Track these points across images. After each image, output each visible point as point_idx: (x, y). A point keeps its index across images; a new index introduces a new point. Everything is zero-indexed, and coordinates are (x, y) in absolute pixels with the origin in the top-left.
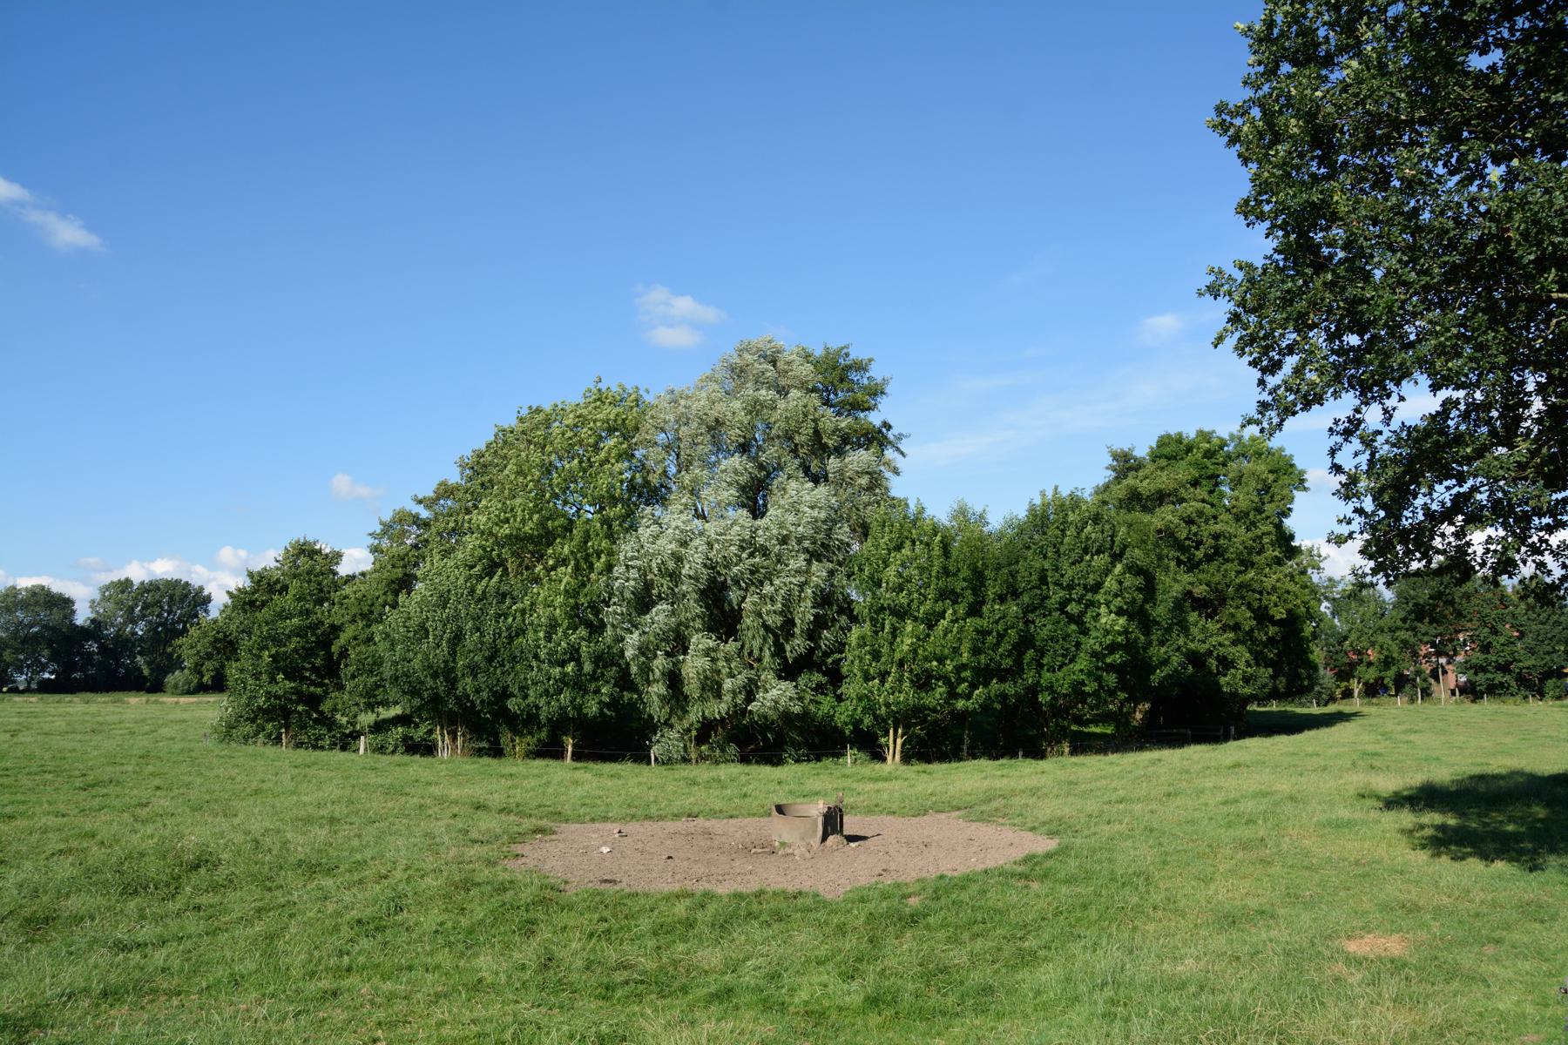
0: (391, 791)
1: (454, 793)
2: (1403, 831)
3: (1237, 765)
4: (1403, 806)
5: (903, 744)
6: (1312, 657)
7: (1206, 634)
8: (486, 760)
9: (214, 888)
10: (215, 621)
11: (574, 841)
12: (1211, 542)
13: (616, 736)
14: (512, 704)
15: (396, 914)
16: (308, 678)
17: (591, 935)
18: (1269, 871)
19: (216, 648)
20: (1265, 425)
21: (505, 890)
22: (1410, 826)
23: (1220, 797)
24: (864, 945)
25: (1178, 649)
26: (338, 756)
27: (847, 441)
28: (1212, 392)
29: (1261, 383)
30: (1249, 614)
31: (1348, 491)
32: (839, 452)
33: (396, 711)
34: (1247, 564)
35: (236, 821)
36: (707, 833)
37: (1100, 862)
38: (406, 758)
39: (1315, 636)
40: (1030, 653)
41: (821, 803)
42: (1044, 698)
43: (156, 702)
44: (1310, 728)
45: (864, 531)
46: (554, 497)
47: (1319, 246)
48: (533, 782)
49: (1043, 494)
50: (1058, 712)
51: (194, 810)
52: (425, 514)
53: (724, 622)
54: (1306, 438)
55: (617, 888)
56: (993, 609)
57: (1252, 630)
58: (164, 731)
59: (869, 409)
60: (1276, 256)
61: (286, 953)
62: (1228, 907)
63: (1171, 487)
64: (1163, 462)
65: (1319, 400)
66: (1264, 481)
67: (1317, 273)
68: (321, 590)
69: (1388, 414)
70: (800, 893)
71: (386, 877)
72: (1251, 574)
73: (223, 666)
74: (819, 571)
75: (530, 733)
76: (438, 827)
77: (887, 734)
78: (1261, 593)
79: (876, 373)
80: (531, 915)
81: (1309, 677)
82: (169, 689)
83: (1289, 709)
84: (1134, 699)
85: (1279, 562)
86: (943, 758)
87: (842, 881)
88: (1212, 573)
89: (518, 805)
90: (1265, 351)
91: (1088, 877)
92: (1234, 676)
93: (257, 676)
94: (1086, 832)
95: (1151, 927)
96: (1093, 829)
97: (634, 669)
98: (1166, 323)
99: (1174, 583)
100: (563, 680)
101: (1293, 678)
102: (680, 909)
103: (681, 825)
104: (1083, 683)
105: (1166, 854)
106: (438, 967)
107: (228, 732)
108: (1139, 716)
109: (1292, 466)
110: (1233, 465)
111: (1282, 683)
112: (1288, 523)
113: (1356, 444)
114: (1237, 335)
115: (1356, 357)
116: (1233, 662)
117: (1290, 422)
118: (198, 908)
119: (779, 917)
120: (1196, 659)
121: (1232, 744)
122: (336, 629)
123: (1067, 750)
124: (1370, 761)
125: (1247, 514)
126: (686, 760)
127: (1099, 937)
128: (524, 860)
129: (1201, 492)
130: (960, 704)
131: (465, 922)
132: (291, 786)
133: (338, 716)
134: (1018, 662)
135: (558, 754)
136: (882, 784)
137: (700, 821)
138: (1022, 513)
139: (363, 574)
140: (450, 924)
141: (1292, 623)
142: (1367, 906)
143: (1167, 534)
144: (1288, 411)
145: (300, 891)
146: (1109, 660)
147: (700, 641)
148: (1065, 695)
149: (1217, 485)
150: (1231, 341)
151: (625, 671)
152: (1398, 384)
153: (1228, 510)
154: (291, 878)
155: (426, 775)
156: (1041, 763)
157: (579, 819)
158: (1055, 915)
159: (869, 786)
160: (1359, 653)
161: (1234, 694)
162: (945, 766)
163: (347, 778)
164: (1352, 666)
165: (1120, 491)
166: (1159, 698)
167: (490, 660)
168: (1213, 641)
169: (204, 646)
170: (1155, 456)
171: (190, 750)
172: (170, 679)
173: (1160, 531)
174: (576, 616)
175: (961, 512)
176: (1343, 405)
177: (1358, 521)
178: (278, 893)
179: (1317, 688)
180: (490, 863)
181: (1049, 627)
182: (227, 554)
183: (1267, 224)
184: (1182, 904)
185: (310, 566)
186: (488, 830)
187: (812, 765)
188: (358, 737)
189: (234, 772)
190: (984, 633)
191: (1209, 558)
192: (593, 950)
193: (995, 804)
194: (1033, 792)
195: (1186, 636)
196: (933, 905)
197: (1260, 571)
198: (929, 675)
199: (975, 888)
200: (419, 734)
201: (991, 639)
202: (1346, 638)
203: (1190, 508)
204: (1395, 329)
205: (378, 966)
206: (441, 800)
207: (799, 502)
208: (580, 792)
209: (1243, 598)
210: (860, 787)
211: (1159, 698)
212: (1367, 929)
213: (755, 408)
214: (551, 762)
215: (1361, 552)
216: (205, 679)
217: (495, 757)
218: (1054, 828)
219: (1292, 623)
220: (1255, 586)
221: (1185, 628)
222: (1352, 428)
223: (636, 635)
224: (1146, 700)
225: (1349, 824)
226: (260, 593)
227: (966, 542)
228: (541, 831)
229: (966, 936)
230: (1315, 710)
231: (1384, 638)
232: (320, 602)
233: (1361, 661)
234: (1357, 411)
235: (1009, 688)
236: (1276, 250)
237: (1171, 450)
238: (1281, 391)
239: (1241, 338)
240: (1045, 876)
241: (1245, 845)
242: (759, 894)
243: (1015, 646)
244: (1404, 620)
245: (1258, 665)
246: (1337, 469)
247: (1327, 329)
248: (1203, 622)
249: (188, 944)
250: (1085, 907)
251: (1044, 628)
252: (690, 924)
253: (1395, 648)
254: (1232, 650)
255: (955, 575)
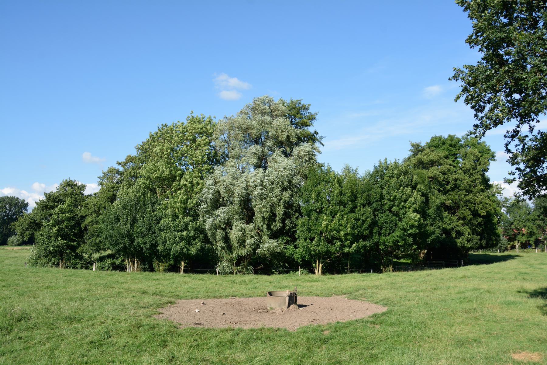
0: (107, 286)
1: (133, 287)
2: (538, 307)
3: (464, 277)
4: (538, 296)
5: (322, 267)
6: (497, 231)
7: (451, 221)
8: (147, 273)
9: (27, 329)
10: (30, 214)
11: (184, 307)
12: (453, 182)
13: (202, 263)
14: (160, 248)
15: (108, 338)
16: (72, 239)
17: (191, 347)
18: (478, 322)
19: (30, 226)
20: (478, 134)
21: (154, 328)
22: (542, 305)
23: (457, 290)
24: (305, 351)
25: (439, 227)
26: (84, 271)
27: (301, 139)
28: (457, 120)
29: (476, 116)
30: (470, 213)
31: (513, 160)
32: (297, 144)
33: (109, 252)
34: (469, 192)
35: (38, 300)
36: (240, 304)
37: (405, 317)
38: (113, 272)
39: (499, 222)
40: (376, 229)
41: (287, 291)
42: (382, 247)
43: (3, 249)
44: (496, 261)
45: (305, 177)
46: (171, 163)
47: (502, 56)
48: (167, 282)
49: (380, 162)
50: (389, 253)
51: (19, 295)
52: (121, 169)
53: (248, 214)
54: (495, 138)
55: (202, 327)
56: (360, 211)
57: (471, 220)
58: (7, 262)
59: (309, 126)
60: (483, 61)
61: (59, 356)
62: (460, 338)
63: (437, 158)
64: (433, 148)
65: (501, 122)
66: (477, 156)
67: (501, 67)
68: (77, 201)
69: (531, 129)
70: (279, 329)
71: (104, 323)
72: (471, 196)
73: (33, 234)
74: (286, 195)
75: (166, 261)
76: (126, 301)
77: (315, 263)
78: (475, 204)
79: (312, 111)
80: (166, 338)
81: (496, 240)
82: (9, 244)
83: (487, 253)
84: (420, 248)
85: (483, 191)
86: (339, 272)
87: (296, 324)
88: (454, 195)
89: (160, 292)
90: (477, 102)
91: (400, 323)
92: (463, 239)
93: (49, 237)
94: (399, 304)
95: (427, 345)
96: (402, 303)
97: (209, 235)
98: (435, 89)
99: (437, 199)
100: (182, 239)
101: (489, 240)
102: (228, 336)
103: (229, 300)
104: (398, 241)
105: (433, 314)
106: (125, 361)
107: (35, 262)
108: (422, 255)
109: (489, 150)
110: (463, 150)
111: (484, 242)
112: (487, 174)
113: (517, 141)
114: (465, 96)
115: (517, 104)
116: (462, 233)
117: (488, 132)
118: (20, 338)
119: (270, 339)
120: (446, 232)
121: (462, 268)
122: (83, 218)
123: (391, 269)
124: (524, 276)
125: (469, 170)
126: (232, 273)
127: (405, 349)
128: (162, 315)
129: (450, 161)
130: (346, 250)
131: (137, 342)
132: (63, 284)
133: (84, 255)
134: (371, 232)
135: (178, 270)
136: (313, 284)
137: (237, 299)
138: (372, 170)
139: (95, 194)
140: (131, 343)
141: (488, 217)
142: (522, 339)
143: (434, 179)
144: (488, 128)
145: (65, 328)
146: (409, 232)
147: (238, 224)
148: (391, 247)
149: (456, 158)
150: (463, 98)
151: (206, 235)
152: (536, 115)
153: (461, 169)
154: (63, 324)
155: (121, 279)
156: (380, 275)
157: (186, 298)
158: (386, 340)
159: (308, 284)
160: (519, 230)
161: (463, 247)
162: (340, 276)
163: (87, 281)
164: (515, 235)
165: (414, 160)
166: (430, 248)
167: (149, 230)
168: (454, 224)
169: (25, 225)
170: (429, 146)
171: (19, 270)
172: (10, 239)
173: (431, 178)
174: (186, 212)
175: (347, 170)
176: (511, 125)
177: (518, 173)
178: (56, 331)
179: (499, 245)
180: (148, 316)
181: (384, 217)
182: (36, 186)
183: (480, 47)
184: (440, 335)
185: (72, 190)
186: (148, 302)
187: (285, 275)
188: (92, 264)
189: (38, 279)
190: (357, 220)
191: (452, 189)
192: (191, 353)
193: (361, 292)
194: (377, 287)
195: (443, 222)
196: (335, 334)
197: (475, 195)
198: (333, 238)
199: (352, 328)
200: (118, 262)
201: (359, 223)
202: (512, 223)
203: (445, 168)
204: (536, 91)
205: (99, 361)
206: (127, 290)
207: (281, 165)
208: (187, 286)
209: (467, 206)
210: (304, 284)
211: (430, 248)
212: (523, 349)
213: (262, 123)
214: (175, 274)
215: (518, 186)
216: (25, 239)
217: (151, 271)
218: (386, 302)
219: (488, 217)
220: (473, 201)
221: (441, 218)
222: (515, 134)
223: (211, 220)
224: (425, 249)
225: (514, 303)
226: (51, 202)
227: (349, 182)
228: (170, 303)
229: (348, 348)
230: (499, 254)
231: (530, 224)
232: (76, 206)
233: (519, 233)
234: (518, 127)
235: (367, 243)
236: (483, 59)
237: (437, 143)
238: (484, 119)
239: (467, 97)
240: (382, 323)
241: (467, 311)
242: (261, 330)
243: (370, 225)
244: (539, 216)
245: (473, 234)
246: (509, 151)
247: (505, 92)
248: (450, 216)
249: (15, 354)
250: (398, 336)
251: (382, 218)
252: (232, 342)
253: (535, 228)
254: (462, 228)
255: (345, 195)
